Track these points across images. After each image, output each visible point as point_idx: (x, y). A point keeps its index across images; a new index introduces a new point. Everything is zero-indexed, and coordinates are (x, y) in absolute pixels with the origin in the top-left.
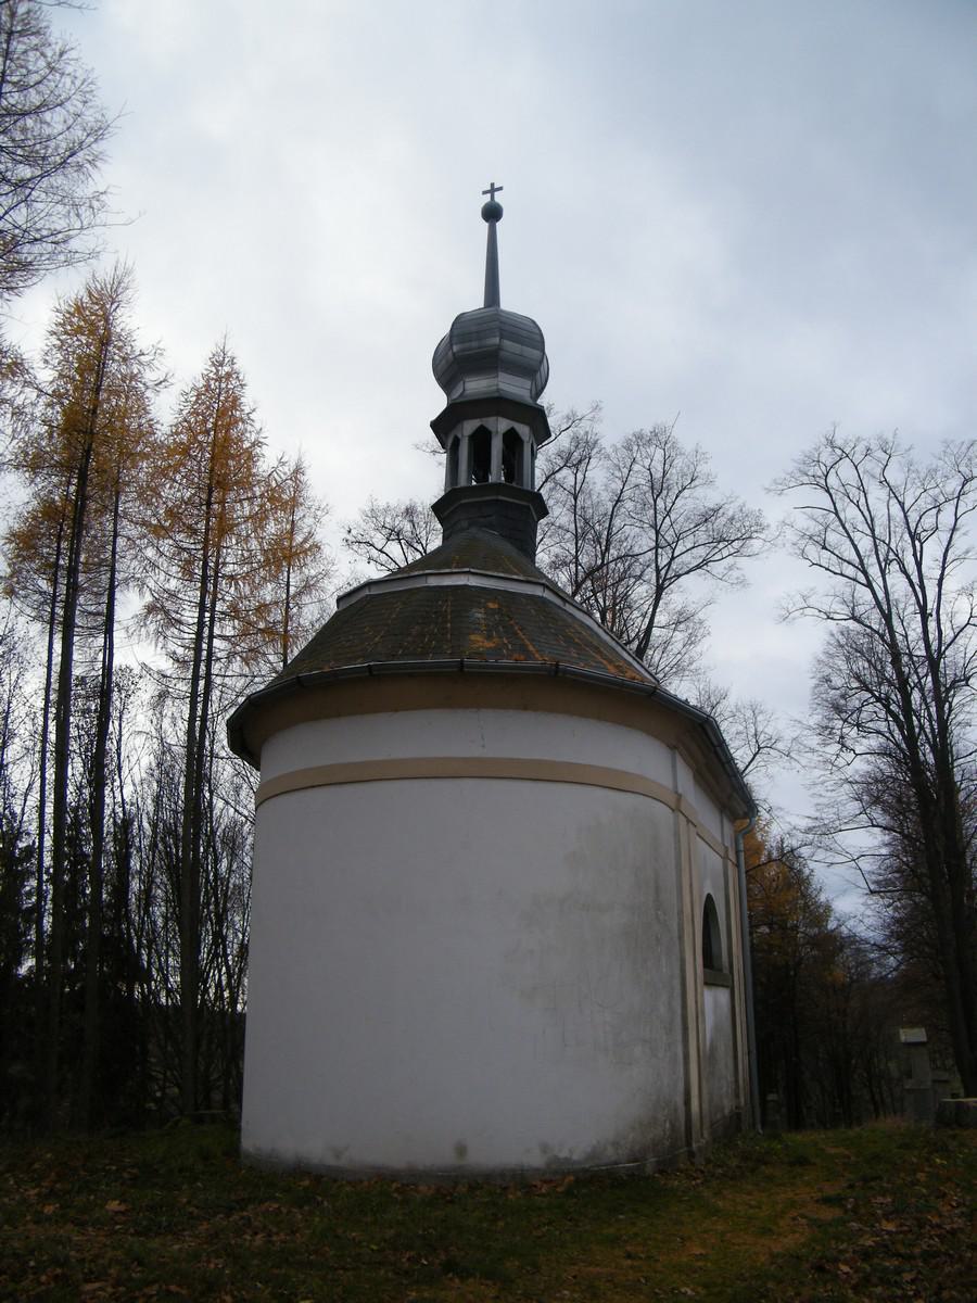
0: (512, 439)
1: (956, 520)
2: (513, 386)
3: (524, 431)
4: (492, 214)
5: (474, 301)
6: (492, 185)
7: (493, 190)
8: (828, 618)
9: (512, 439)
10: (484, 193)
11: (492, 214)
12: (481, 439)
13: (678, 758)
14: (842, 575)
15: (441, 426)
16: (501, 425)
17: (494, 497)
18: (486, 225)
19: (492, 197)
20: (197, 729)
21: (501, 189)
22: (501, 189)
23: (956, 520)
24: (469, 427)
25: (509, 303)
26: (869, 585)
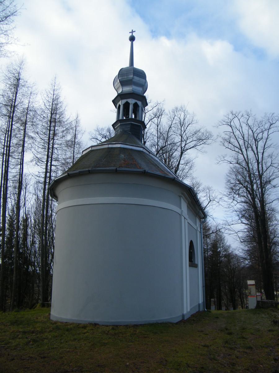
0: (136, 106)
1: (268, 135)
2: (138, 90)
3: (139, 103)
4: (132, 39)
5: (126, 65)
6: (132, 30)
7: (132, 32)
8: (231, 163)
9: (136, 106)
10: (130, 33)
11: (132, 39)
12: (126, 106)
13: (182, 200)
14: (235, 151)
15: (115, 102)
16: (132, 101)
17: (130, 122)
18: (130, 42)
19: (132, 34)
20: (45, 213)
21: (135, 31)
22: (135, 31)
23: (268, 135)
24: (124, 101)
25: (137, 65)
26: (242, 154)
